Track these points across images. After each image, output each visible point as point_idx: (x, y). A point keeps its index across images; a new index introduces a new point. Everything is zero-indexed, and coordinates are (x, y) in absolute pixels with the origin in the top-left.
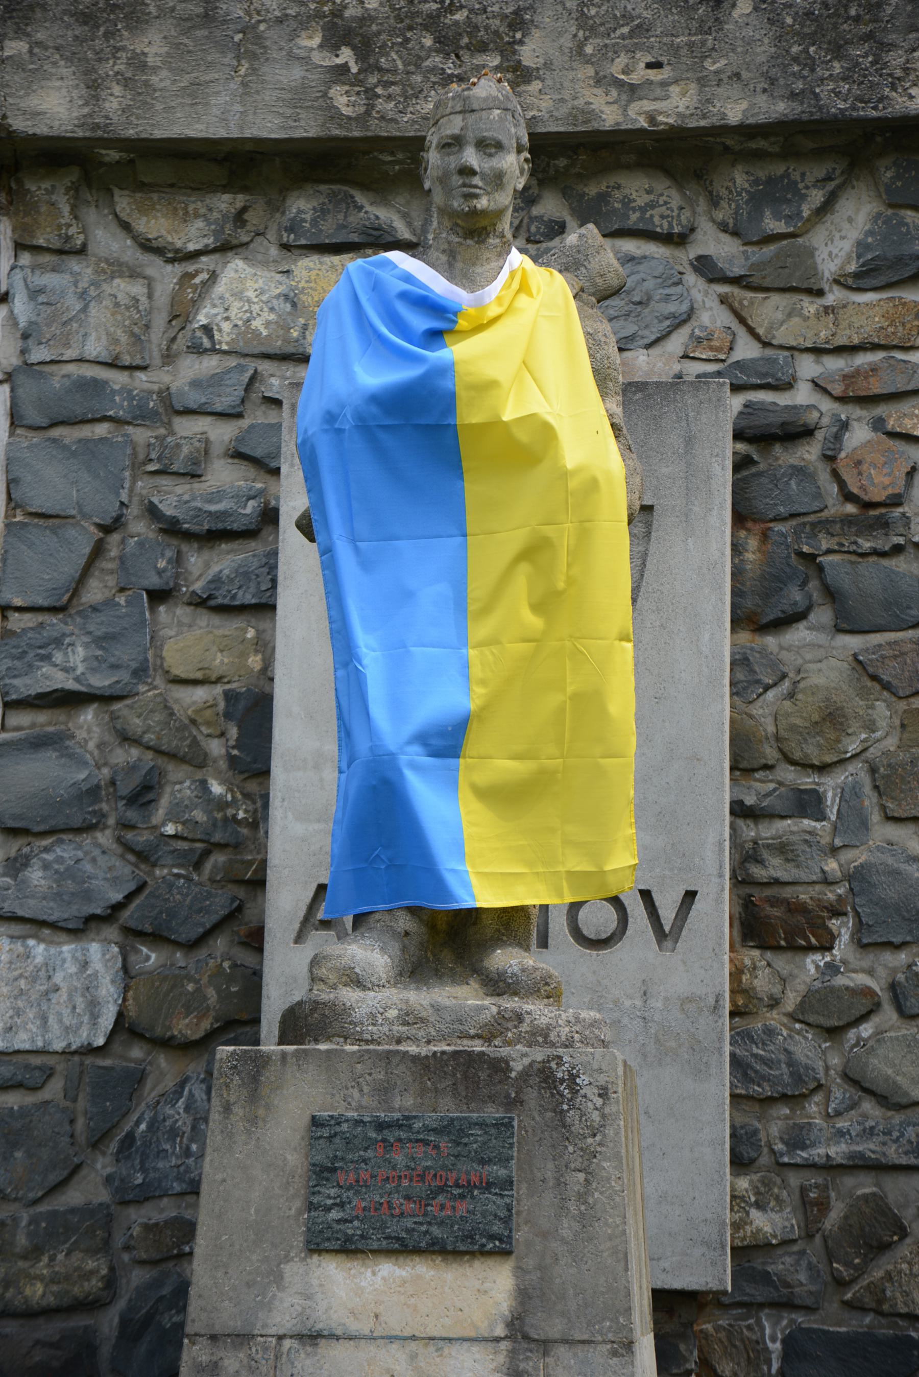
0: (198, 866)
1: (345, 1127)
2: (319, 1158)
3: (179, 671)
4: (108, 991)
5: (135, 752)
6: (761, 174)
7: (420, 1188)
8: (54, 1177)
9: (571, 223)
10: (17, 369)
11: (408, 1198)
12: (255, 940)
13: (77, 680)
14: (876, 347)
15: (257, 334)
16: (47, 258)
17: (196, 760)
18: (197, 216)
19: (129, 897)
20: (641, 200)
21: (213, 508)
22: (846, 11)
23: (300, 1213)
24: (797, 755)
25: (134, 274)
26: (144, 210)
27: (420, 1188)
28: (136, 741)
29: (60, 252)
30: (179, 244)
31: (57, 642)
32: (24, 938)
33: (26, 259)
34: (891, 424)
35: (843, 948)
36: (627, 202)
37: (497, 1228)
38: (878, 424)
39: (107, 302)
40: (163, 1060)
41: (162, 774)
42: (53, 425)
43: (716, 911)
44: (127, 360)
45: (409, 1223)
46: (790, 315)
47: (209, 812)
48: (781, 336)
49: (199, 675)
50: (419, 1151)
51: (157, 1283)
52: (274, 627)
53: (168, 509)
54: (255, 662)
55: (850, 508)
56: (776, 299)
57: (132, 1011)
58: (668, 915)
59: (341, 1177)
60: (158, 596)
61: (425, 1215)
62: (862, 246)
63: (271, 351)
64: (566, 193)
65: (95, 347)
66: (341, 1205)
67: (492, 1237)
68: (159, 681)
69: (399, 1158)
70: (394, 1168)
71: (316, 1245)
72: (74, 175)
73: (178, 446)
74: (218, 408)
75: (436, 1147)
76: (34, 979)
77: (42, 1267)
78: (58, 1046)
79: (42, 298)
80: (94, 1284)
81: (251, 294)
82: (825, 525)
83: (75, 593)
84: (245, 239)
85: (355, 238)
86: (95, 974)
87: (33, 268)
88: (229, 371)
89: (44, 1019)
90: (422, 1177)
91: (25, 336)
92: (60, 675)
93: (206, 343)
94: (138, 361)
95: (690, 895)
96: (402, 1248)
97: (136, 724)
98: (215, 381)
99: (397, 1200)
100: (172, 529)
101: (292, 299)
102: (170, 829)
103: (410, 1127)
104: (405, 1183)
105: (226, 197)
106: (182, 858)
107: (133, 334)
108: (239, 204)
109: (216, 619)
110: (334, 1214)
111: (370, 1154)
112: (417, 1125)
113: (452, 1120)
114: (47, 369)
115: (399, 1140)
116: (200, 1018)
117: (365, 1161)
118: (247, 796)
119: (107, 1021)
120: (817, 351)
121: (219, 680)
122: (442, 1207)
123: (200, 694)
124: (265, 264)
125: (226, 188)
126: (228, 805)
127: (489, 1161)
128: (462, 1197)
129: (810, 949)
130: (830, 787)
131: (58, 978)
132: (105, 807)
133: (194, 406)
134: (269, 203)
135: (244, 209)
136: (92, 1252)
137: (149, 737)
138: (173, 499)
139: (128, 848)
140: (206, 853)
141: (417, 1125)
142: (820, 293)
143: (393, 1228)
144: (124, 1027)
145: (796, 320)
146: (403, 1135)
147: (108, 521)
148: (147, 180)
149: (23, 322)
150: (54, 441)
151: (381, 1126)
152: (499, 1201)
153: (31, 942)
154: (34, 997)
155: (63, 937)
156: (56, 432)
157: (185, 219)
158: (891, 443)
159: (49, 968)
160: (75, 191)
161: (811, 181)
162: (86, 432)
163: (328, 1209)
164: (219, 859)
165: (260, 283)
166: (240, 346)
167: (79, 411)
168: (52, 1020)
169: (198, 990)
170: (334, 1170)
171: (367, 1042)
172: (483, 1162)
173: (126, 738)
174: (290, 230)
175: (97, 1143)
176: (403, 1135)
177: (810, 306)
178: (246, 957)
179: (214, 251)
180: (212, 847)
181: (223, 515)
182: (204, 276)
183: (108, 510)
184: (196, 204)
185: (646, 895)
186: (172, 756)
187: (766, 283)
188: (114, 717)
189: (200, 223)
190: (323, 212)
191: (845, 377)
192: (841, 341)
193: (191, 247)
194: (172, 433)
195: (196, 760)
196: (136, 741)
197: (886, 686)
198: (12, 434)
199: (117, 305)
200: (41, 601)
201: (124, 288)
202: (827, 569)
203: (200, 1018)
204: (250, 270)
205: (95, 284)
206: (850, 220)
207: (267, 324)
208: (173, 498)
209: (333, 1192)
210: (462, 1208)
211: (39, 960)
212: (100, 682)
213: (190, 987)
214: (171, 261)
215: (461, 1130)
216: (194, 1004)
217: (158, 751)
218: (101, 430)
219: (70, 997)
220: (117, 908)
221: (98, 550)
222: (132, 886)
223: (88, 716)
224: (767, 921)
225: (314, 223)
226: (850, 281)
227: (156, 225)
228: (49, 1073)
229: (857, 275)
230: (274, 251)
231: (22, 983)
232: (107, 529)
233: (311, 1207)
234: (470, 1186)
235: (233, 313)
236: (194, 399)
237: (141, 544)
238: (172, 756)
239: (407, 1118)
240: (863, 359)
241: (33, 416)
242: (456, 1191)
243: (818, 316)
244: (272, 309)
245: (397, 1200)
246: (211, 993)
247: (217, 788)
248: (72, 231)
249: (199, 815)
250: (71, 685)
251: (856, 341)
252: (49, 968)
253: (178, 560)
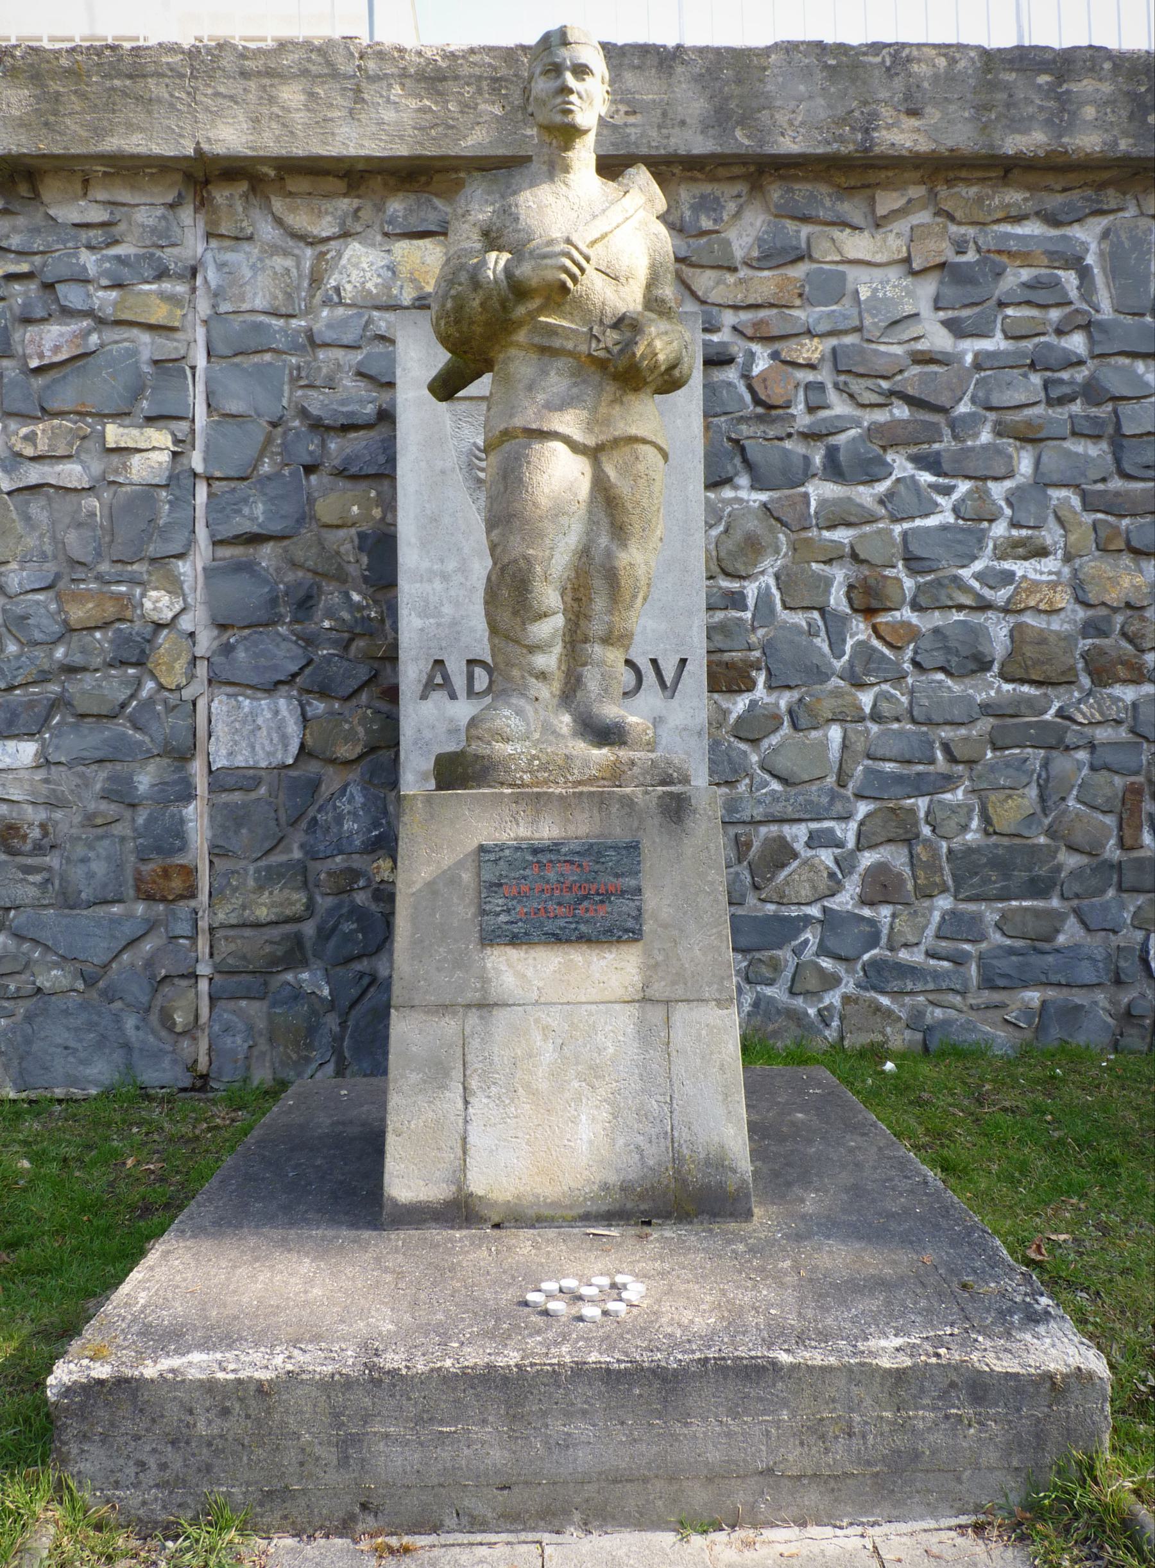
0: (346, 648)
1: (507, 852)
2: (487, 876)
3: (326, 519)
4: (293, 728)
5: (300, 574)
6: (697, 192)
7: (568, 897)
10: (210, 317)
11: (560, 904)
12: (392, 694)
13: (259, 525)
14: (772, 305)
15: (369, 292)
16: (227, 243)
17: (341, 577)
18: (327, 213)
19: (302, 669)
21: (345, 409)
22: (21, 655)
23: (475, 916)
24: (730, 570)
25: (286, 253)
26: (293, 210)
27: (568, 897)
28: (301, 566)
29: (237, 239)
30: (315, 232)
31: (245, 501)
32: (235, 695)
33: (214, 244)
34: (783, 355)
35: (760, 691)
37: (630, 924)
38: (775, 356)
39: (269, 272)
40: (330, 770)
41: (319, 588)
42: (235, 355)
43: (698, 670)
44: (283, 311)
45: (562, 922)
46: (718, 283)
47: (351, 613)
48: (713, 297)
49: (339, 522)
50: (566, 868)
52: (394, 488)
53: (314, 410)
54: (377, 513)
55: (760, 410)
56: (709, 273)
57: (309, 741)
58: (669, 676)
59: (504, 889)
60: (310, 469)
61: (574, 916)
62: (760, 241)
63: (378, 303)
65: (260, 303)
66: (508, 911)
67: (626, 931)
68: (314, 526)
69: (551, 875)
70: (548, 882)
71: (489, 938)
72: (244, 186)
73: (319, 368)
74: (345, 342)
75: (580, 866)
76: (244, 722)
78: (263, 764)
79: (226, 269)
81: (365, 266)
82: (742, 420)
83: (255, 468)
84: (359, 229)
85: (433, 228)
86: (283, 719)
87: (220, 249)
88: (351, 316)
89: (253, 748)
90: (570, 889)
91: (216, 295)
92: (248, 523)
93: (336, 299)
94: (290, 312)
95: (683, 661)
97: (299, 555)
98: (344, 323)
99: (551, 906)
100: (318, 426)
101: (392, 269)
103: (558, 851)
104: (557, 893)
105: (346, 200)
107: (286, 293)
108: (355, 206)
109: (349, 485)
110: (503, 918)
111: (528, 872)
112: (564, 850)
113: (592, 845)
114: (231, 317)
115: (551, 861)
116: (354, 746)
117: (525, 878)
118: (376, 602)
119: (294, 748)
120: (736, 308)
121: (353, 525)
122: (587, 910)
123: (342, 533)
124: (373, 245)
125: (345, 195)
126: (364, 608)
127: (623, 875)
128: (602, 902)
129: (741, 691)
130: (751, 590)
131: (260, 721)
132: (282, 610)
133: (328, 341)
134: (375, 205)
135: (358, 209)
137: (310, 563)
138: (318, 405)
140: (351, 640)
141: (564, 850)
142: (734, 270)
145: (722, 286)
146: (553, 857)
147: (275, 420)
148: (293, 189)
149: (213, 284)
150: (237, 365)
151: (535, 851)
152: (631, 904)
153: (241, 698)
154: (245, 733)
155: (259, 695)
156: (237, 360)
157: (320, 215)
158: (784, 367)
159: (253, 715)
160: (245, 196)
161: (728, 193)
162: (256, 359)
163: (498, 914)
164: (361, 643)
165: (371, 258)
166: (360, 302)
167: (253, 346)
168: (258, 748)
169: (352, 728)
170: (500, 885)
171: (519, 786)
172: (617, 876)
173: (294, 565)
174: (390, 223)
176: (553, 857)
177: (730, 279)
178: (384, 706)
179: (339, 237)
182: (333, 253)
183: (274, 412)
184: (327, 205)
185: (654, 662)
186: (325, 575)
187: (704, 262)
189: (329, 218)
190: (410, 211)
191: (754, 325)
192: (751, 301)
193: (324, 234)
194: (316, 359)
195: (341, 577)
196: (301, 566)
197: (784, 524)
198: (209, 362)
199: (275, 273)
200: (232, 474)
201: (280, 262)
202: (748, 450)
203: (354, 746)
204: (364, 250)
205: (261, 260)
206: (751, 224)
207: (376, 286)
208: (316, 402)
209: (500, 901)
211: (246, 710)
212: (276, 527)
213: (347, 726)
214: (312, 244)
215: (599, 852)
216: (350, 737)
217: (316, 573)
218: (268, 357)
219: (269, 734)
220: (294, 676)
221: (269, 440)
222: (304, 662)
223: (267, 549)
224: (726, 677)
225: (405, 217)
226: (754, 264)
227: (300, 220)
229: (759, 259)
230: (379, 238)
231: (237, 725)
232: (274, 425)
233: (484, 913)
234: (608, 894)
235: (353, 278)
236: (329, 336)
237: (297, 435)
238: (325, 575)
239: (556, 844)
240: (763, 314)
241: (221, 348)
242: (597, 898)
243: (735, 284)
244: (379, 276)
245: (551, 906)
246: (361, 730)
247: (356, 597)
248: (245, 224)
250: (255, 529)
251: (760, 301)
252: (253, 715)
253: (323, 445)
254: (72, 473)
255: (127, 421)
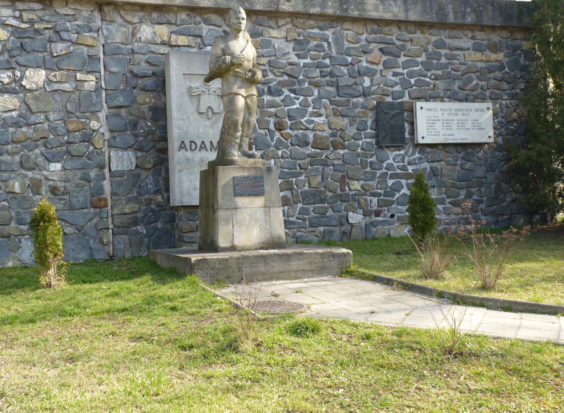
3: (140, 102)
4: (134, 160)
5: (133, 117)
8: (128, 192)
9: (202, 23)
16: (108, 23)
17: (144, 118)
20: (214, 19)
25: (125, 27)
26: (127, 14)
36: (212, 19)
40: (143, 171)
44: (125, 43)
51: (147, 209)
53: (135, 71)
64: (200, 16)
77: (128, 206)
78: (126, 170)
80: (137, 209)
96: (249, 195)
97: (133, 112)
98: (142, 48)
101: (154, 33)
102: (141, 131)
105: (142, 13)
106: (144, 136)
109: (145, 93)
124: (148, 25)
125: (140, 11)
131: (124, 158)
136: (136, 204)
137: (136, 114)
139: (133, 134)
143: (248, 192)
144: (137, 166)
156: (112, 56)
159: (122, 156)
162: (118, 56)
173: (131, 114)
175: (134, 186)
180: (149, 134)
181: (144, 73)
186: (140, 118)
188: (128, 110)
195: (144, 118)
200: (113, 89)
201: (123, 29)
210: (257, 189)
216: (149, 162)
217: (138, 117)
218: (121, 56)
227: (129, 18)
228: (124, 174)
230: (150, 24)
236: (138, 51)
238: (140, 118)
247: (149, 124)
249: (146, 129)
250: (121, 104)
254: (67, 87)
255: (82, 72)
